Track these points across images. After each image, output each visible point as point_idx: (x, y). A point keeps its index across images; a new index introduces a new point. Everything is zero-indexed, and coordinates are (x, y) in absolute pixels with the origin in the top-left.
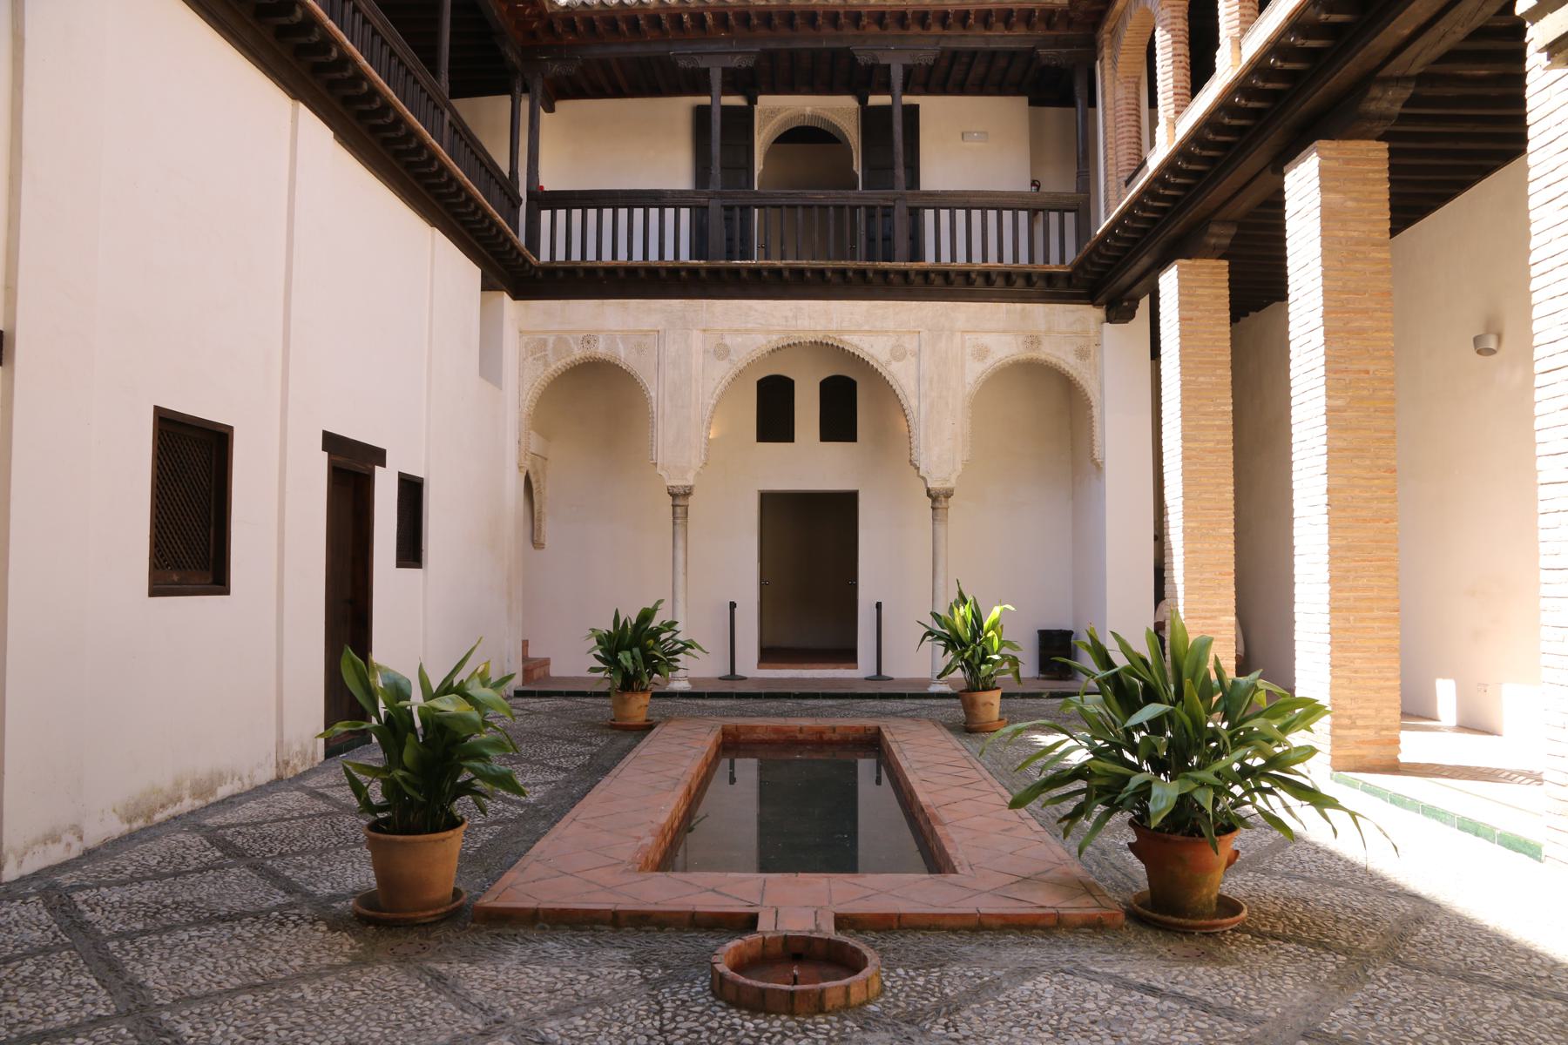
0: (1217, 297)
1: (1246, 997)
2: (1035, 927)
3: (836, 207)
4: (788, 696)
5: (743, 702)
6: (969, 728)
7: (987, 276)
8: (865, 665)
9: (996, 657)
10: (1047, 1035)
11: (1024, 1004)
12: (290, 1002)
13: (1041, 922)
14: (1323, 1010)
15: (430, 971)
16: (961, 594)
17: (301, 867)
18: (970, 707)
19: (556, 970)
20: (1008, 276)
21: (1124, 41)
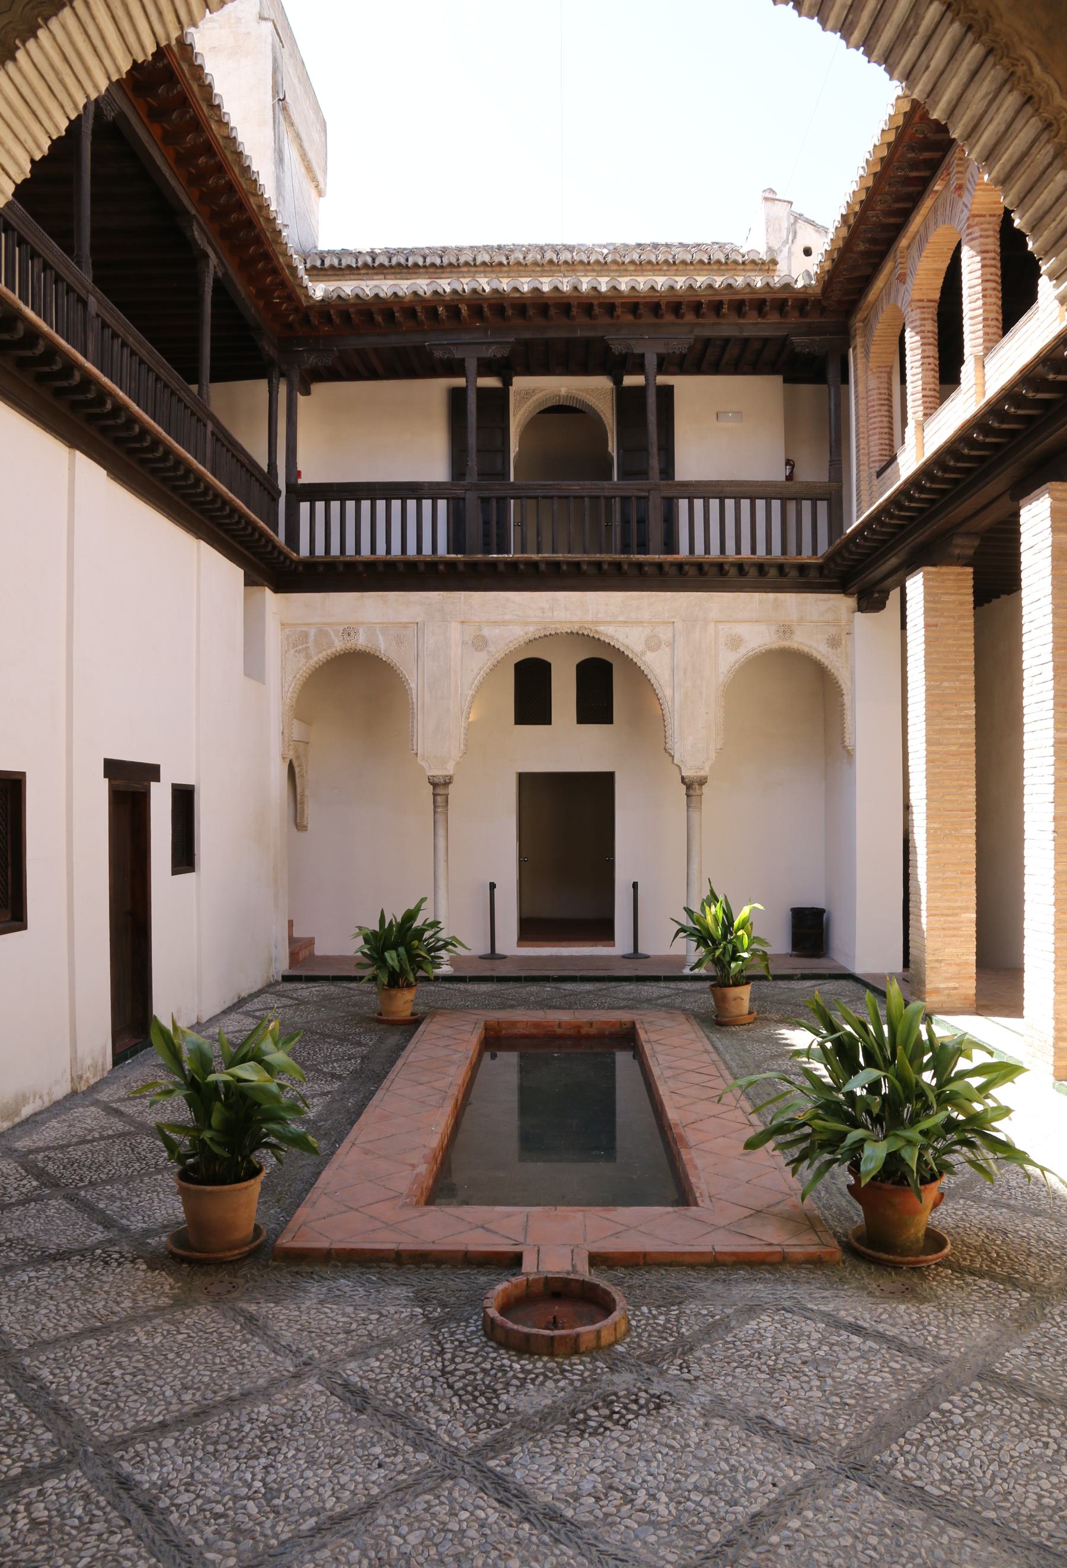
0: (962, 603)
1: (936, 1337)
2: (762, 1263)
3: (591, 497)
4: (547, 979)
5: (503, 987)
6: (718, 1020)
7: (740, 567)
8: (622, 944)
9: (745, 955)
10: (764, 1376)
11: (748, 1344)
12: (129, 1346)
13: (768, 1259)
14: (1000, 1350)
15: (242, 1311)
16: (712, 891)
17: (112, 1198)
18: (721, 1001)
19: (349, 1310)
20: (761, 568)
21: (877, 333)
